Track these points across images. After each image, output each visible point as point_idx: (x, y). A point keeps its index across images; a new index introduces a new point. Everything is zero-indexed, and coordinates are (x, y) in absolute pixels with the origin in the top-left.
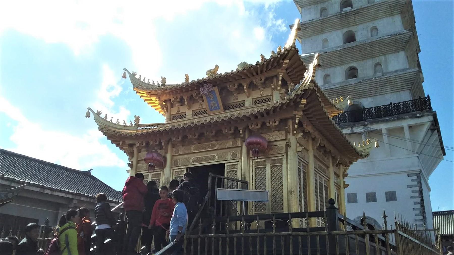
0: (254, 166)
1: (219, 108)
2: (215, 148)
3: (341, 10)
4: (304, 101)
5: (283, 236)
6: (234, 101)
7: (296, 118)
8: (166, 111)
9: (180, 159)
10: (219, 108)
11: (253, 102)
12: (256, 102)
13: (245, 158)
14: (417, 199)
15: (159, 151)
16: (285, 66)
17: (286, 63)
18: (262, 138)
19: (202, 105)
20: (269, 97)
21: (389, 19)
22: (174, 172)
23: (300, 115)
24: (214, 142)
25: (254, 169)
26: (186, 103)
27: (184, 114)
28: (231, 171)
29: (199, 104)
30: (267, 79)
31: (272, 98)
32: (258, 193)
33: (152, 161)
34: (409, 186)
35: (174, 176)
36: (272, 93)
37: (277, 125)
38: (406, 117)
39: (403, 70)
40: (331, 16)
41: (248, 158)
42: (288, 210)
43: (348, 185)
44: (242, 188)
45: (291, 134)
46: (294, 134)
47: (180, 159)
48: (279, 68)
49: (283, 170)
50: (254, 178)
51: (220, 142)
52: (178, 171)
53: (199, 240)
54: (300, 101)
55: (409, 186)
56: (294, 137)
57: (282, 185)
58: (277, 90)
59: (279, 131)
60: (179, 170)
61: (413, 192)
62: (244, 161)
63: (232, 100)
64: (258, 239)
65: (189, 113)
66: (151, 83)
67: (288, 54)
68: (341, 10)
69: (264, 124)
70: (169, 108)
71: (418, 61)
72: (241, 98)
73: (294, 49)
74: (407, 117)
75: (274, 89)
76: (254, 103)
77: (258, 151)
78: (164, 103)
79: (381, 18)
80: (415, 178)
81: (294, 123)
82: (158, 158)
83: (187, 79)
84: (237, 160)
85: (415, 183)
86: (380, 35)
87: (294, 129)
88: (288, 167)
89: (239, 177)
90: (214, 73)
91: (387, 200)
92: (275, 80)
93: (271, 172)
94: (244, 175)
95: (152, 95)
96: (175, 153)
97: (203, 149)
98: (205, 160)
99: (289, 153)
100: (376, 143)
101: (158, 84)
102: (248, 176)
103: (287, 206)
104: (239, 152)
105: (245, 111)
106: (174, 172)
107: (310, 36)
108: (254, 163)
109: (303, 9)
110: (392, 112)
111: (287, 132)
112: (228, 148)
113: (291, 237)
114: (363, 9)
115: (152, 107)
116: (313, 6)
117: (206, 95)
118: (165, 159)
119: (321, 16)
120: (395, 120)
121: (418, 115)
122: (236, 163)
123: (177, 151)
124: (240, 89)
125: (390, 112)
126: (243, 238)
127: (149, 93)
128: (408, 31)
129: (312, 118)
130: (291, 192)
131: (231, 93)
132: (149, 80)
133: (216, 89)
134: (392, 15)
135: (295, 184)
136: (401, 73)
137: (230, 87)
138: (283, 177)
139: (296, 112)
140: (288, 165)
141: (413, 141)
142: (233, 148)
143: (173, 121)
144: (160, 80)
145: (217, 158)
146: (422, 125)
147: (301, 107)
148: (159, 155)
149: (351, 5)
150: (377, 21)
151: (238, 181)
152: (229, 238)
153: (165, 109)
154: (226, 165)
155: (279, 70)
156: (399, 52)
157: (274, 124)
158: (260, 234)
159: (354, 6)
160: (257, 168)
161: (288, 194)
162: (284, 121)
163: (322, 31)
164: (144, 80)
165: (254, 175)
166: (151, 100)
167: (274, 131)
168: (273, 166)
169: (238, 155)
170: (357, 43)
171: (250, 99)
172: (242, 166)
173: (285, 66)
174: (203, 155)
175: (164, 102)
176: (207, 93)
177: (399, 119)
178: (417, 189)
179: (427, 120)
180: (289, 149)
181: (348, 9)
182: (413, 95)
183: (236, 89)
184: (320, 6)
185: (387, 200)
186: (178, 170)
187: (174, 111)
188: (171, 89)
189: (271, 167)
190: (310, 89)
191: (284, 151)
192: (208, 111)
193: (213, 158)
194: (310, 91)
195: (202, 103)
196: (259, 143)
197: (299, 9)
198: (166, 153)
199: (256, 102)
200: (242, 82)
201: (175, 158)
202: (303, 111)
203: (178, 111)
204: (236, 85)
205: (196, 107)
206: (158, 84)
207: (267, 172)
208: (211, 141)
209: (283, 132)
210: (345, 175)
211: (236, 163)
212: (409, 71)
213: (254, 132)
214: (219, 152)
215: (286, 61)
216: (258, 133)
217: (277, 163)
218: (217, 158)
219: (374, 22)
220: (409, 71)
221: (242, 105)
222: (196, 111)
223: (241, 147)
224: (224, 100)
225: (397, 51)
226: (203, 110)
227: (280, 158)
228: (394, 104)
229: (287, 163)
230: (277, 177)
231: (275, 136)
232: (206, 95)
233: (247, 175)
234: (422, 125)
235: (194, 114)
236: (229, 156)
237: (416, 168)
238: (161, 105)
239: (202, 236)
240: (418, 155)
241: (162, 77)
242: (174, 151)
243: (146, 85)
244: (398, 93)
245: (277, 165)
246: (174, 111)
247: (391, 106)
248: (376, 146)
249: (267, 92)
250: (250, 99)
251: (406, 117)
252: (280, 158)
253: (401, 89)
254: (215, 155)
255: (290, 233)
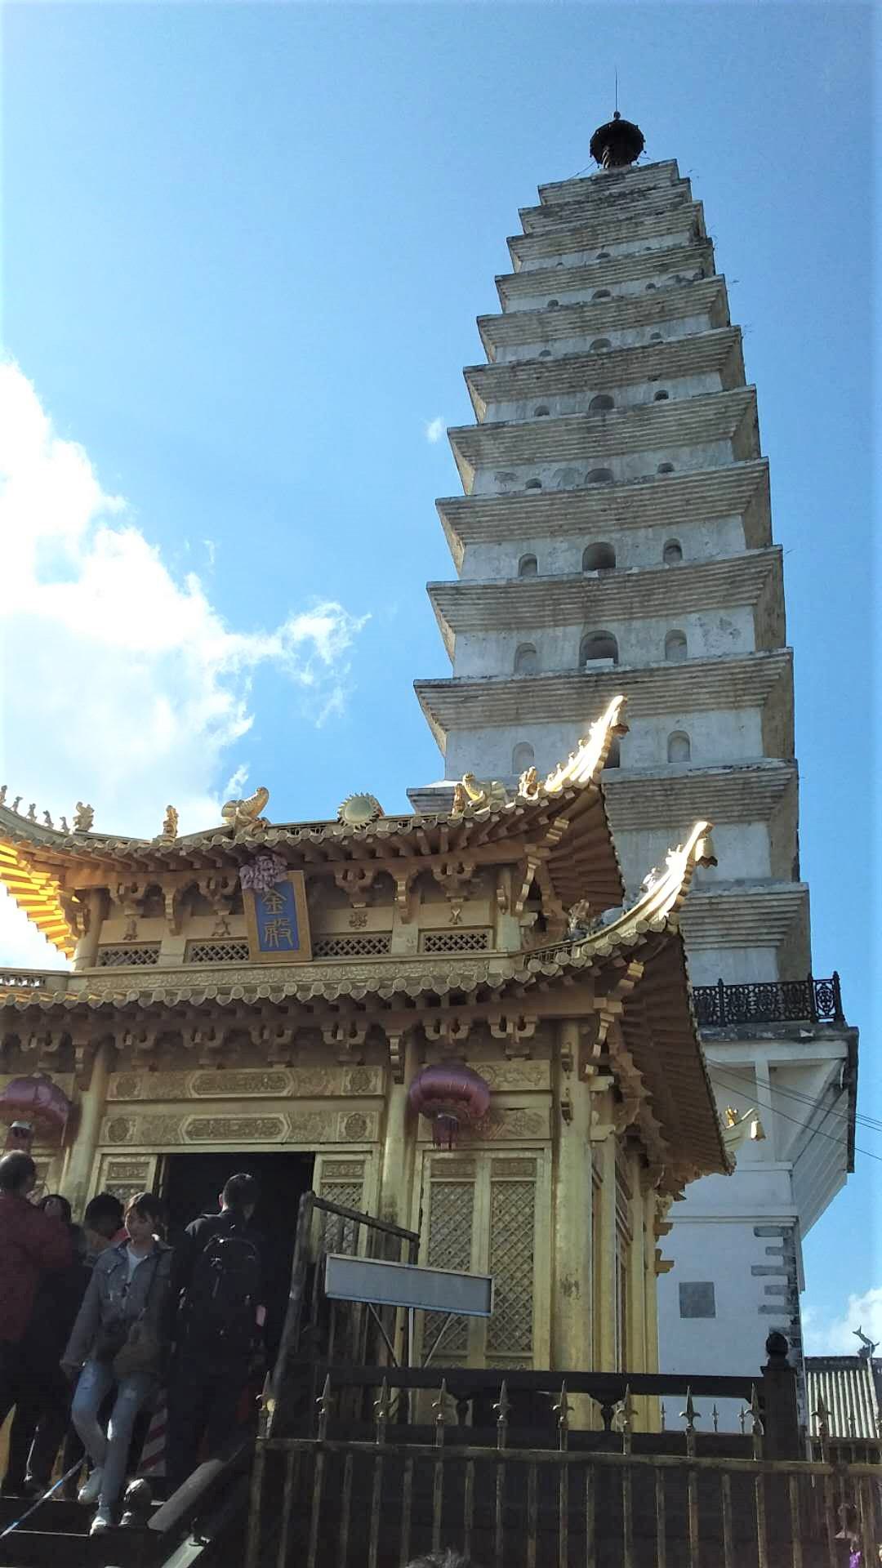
0: (427, 1173)
1: (296, 947)
2: (284, 1094)
3: (583, 664)
4: (636, 969)
5: (662, 1467)
6: (353, 930)
7: (599, 1020)
8: (81, 927)
9: (139, 1120)
10: (296, 947)
11: (423, 941)
12: (433, 943)
13: (395, 1141)
14: (781, 1317)
15: (56, 1078)
16: (553, 837)
17: (559, 829)
18: (473, 1075)
19: (227, 925)
20: (481, 932)
21: (729, 716)
22: (106, 1166)
23: (615, 1015)
24: (279, 1068)
25: (427, 1187)
26: (169, 910)
27: (154, 947)
28: (336, 1185)
29: (213, 920)
30: (479, 869)
31: (490, 937)
32: (458, 1282)
33: (29, 1114)
34: (758, 1271)
35: (103, 1180)
36: (494, 919)
37: (531, 1038)
38: (765, 1035)
39: (761, 882)
40: (551, 674)
41: (406, 1143)
42: (624, 1365)
43: (671, 1263)
44: (373, 1252)
45: (574, 1075)
46: (584, 1078)
47: (138, 1119)
48: (530, 841)
49: (537, 1200)
50: (425, 1219)
51: (302, 1072)
52: (124, 1165)
53: (320, 1459)
54: (626, 968)
55: (758, 1271)
56: (582, 1085)
57: (531, 1257)
58: (514, 913)
59: (529, 1057)
60: (128, 1160)
61: (768, 1290)
62: (394, 1152)
63: (341, 924)
64: (564, 1473)
65: (172, 949)
66: (41, 820)
67: (573, 800)
68: (583, 664)
69: (480, 1027)
70: (94, 917)
71: (797, 858)
72: (378, 920)
73: (595, 788)
74: (770, 1035)
75: (504, 907)
76: (423, 947)
77: (452, 1121)
78: (74, 899)
79: (702, 711)
80: (778, 1242)
81: (587, 1041)
82: (55, 1107)
83: (170, 826)
84: (366, 1147)
85: (777, 1261)
86: (695, 762)
87: (586, 1058)
88: (559, 1193)
89: (368, 1205)
90: (249, 814)
91: (684, 1315)
92: (506, 878)
93: (492, 1204)
94: (393, 1204)
95: (35, 863)
96: (119, 1093)
97: (233, 1090)
98: (239, 1134)
99: (563, 1141)
100: (754, 1125)
101: (65, 826)
102: (405, 1211)
103: (547, 1336)
104: (376, 1115)
105: (381, 971)
106: (106, 1166)
107: (475, 727)
108: (428, 1164)
109: (462, 639)
110: (722, 1011)
111: (560, 1064)
112: (333, 1098)
113: (693, 1475)
114: (651, 672)
115: (19, 904)
116: (493, 635)
117: (258, 896)
118: (76, 1113)
119: (516, 669)
120: (732, 1040)
121: (804, 1034)
122: (360, 1157)
123: (126, 1087)
124: (380, 890)
125: (714, 1012)
126: (501, 1468)
127: (30, 856)
128: (782, 765)
129: (637, 1025)
130: (567, 1288)
131: (342, 897)
132: (32, 807)
133: (298, 878)
134: (736, 706)
135: (582, 1259)
136: (753, 891)
137: (347, 879)
138: (538, 1227)
139: (600, 1003)
140: (560, 1187)
141: (783, 1116)
142: (353, 1098)
143: (105, 970)
144: (72, 814)
145: (286, 1130)
146: (812, 1067)
147: (622, 989)
148: (57, 1092)
149: (612, 653)
150: (689, 716)
151: (359, 1218)
152: (445, 1462)
153: (80, 920)
154: (319, 1159)
155: (530, 848)
156: (750, 823)
157: (519, 1034)
158: (573, 1456)
159: (622, 657)
160: (439, 1184)
161: (553, 1291)
162: (552, 1027)
163: (517, 719)
164: (16, 805)
165: (426, 1210)
166: (27, 880)
167: (509, 1058)
168: (501, 1183)
169: (372, 1128)
170: (625, 774)
171: (413, 928)
172: (384, 1168)
173: (553, 837)
174: (232, 1113)
175: (77, 893)
176: (267, 889)
177: (745, 1038)
178: (783, 1280)
179: (830, 1051)
180: (564, 1129)
181: (606, 663)
182: (782, 969)
183: (363, 889)
184: (516, 639)
185: (684, 1315)
186: (121, 1160)
187: (114, 932)
188: (129, 855)
189: (492, 1183)
190: (670, 933)
191: (545, 1131)
192: (254, 948)
193: (272, 1127)
194: (665, 941)
195: (231, 919)
196: (466, 1097)
197: (445, 636)
198: (85, 1088)
199: (433, 943)
200: (390, 866)
201: (115, 1111)
202: (625, 1001)
203: (128, 936)
204: (369, 875)
205: (203, 929)
206: (65, 826)
207: (477, 1203)
208: (271, 1065)
209: (545, 1065)
210: (661, 1229)
211: (360, 1157)
212: (778, 887)
213: (433, 1048)
214: (294, 1106)
215: (561, 823)
216: (454, 1060)
217: (515, 1175)
218: (286, 1130)
219: (679, 717)
220: (778, 887)
221: (379, 945)
222: (200, 945)
223: (385, 1099)
224: (315, 922)
225: (744, 819)
226: (227, 944)
227: (528, 1155)
228: (731, 987)
229: (555, 1179)
230: (514, 1224)
231: (515, 1075)
232: (258, 896)
233: (401, 1203)
234: (812, 1067)
235: (191, 953)
236: (337, 1128)
237: (784, 1212)
238: (66, 904)
239: (332, 1445)
240: (789, 1166)
241: (80, 804)
242: (113, 1086)
243: (22, 824)
244: (742, 951)
245: (515, 1181)
246: (114, 932)
247: (721, 993)
248: (753, 1134)
249: (475, 915)
250: (413, 928)
251: (765, 1035)
252: (528, 1155)
253: (751, 941)
254: (281, 1117)
255: (690, 1458)
